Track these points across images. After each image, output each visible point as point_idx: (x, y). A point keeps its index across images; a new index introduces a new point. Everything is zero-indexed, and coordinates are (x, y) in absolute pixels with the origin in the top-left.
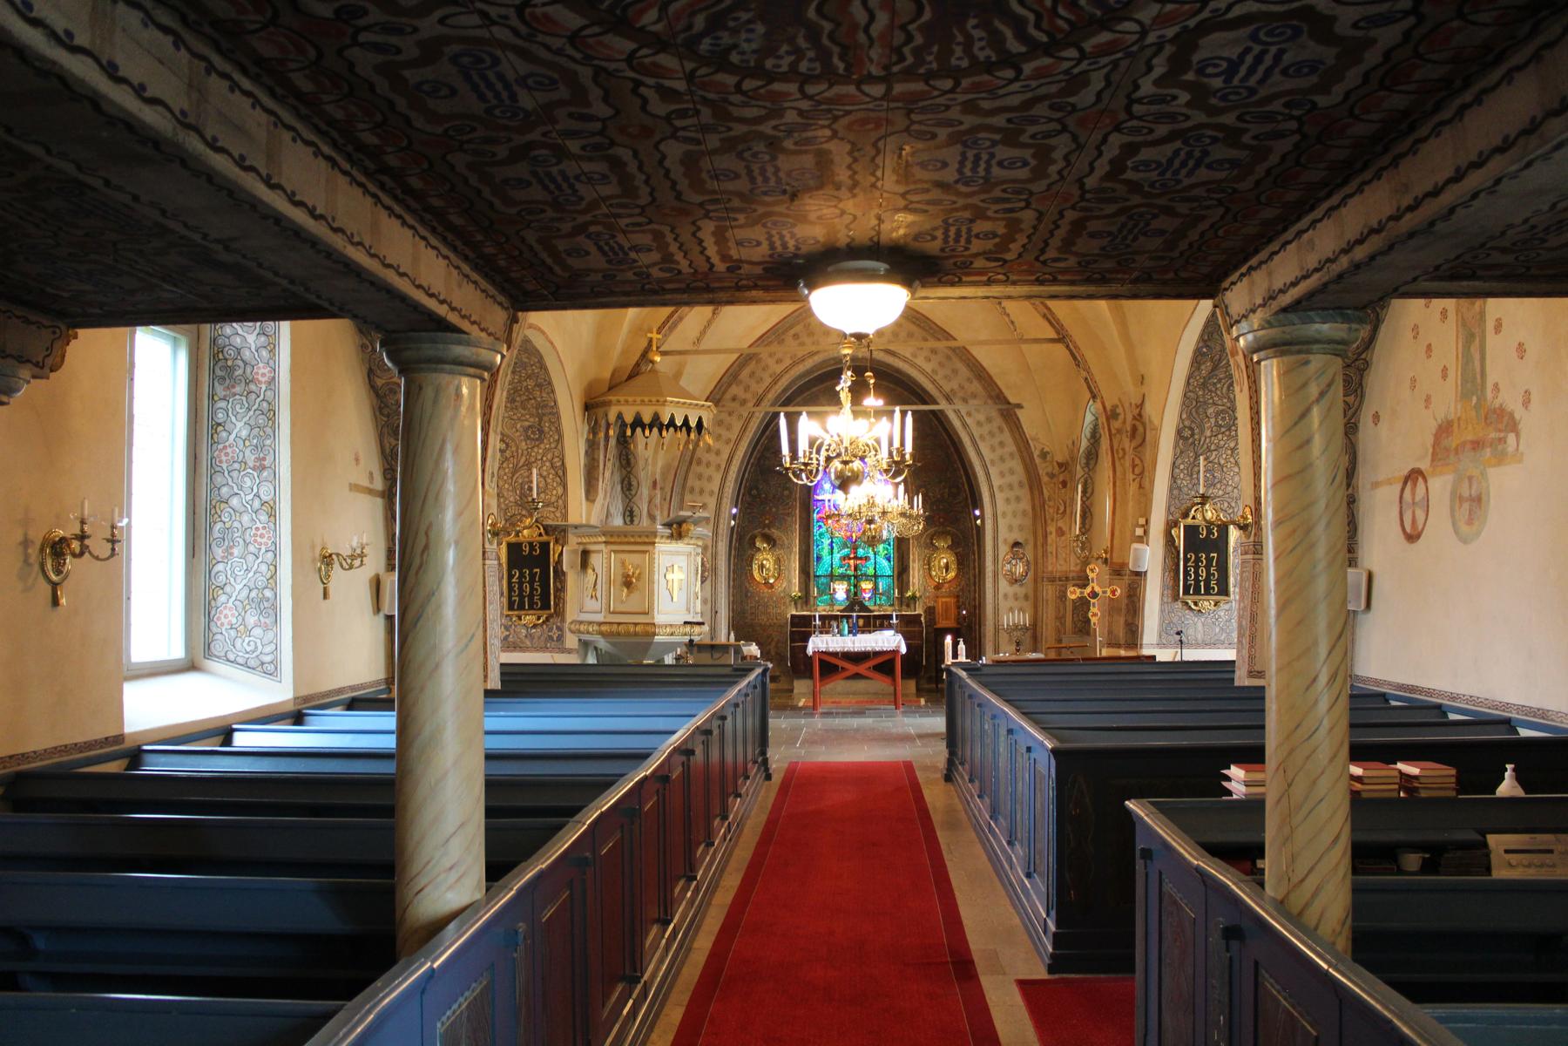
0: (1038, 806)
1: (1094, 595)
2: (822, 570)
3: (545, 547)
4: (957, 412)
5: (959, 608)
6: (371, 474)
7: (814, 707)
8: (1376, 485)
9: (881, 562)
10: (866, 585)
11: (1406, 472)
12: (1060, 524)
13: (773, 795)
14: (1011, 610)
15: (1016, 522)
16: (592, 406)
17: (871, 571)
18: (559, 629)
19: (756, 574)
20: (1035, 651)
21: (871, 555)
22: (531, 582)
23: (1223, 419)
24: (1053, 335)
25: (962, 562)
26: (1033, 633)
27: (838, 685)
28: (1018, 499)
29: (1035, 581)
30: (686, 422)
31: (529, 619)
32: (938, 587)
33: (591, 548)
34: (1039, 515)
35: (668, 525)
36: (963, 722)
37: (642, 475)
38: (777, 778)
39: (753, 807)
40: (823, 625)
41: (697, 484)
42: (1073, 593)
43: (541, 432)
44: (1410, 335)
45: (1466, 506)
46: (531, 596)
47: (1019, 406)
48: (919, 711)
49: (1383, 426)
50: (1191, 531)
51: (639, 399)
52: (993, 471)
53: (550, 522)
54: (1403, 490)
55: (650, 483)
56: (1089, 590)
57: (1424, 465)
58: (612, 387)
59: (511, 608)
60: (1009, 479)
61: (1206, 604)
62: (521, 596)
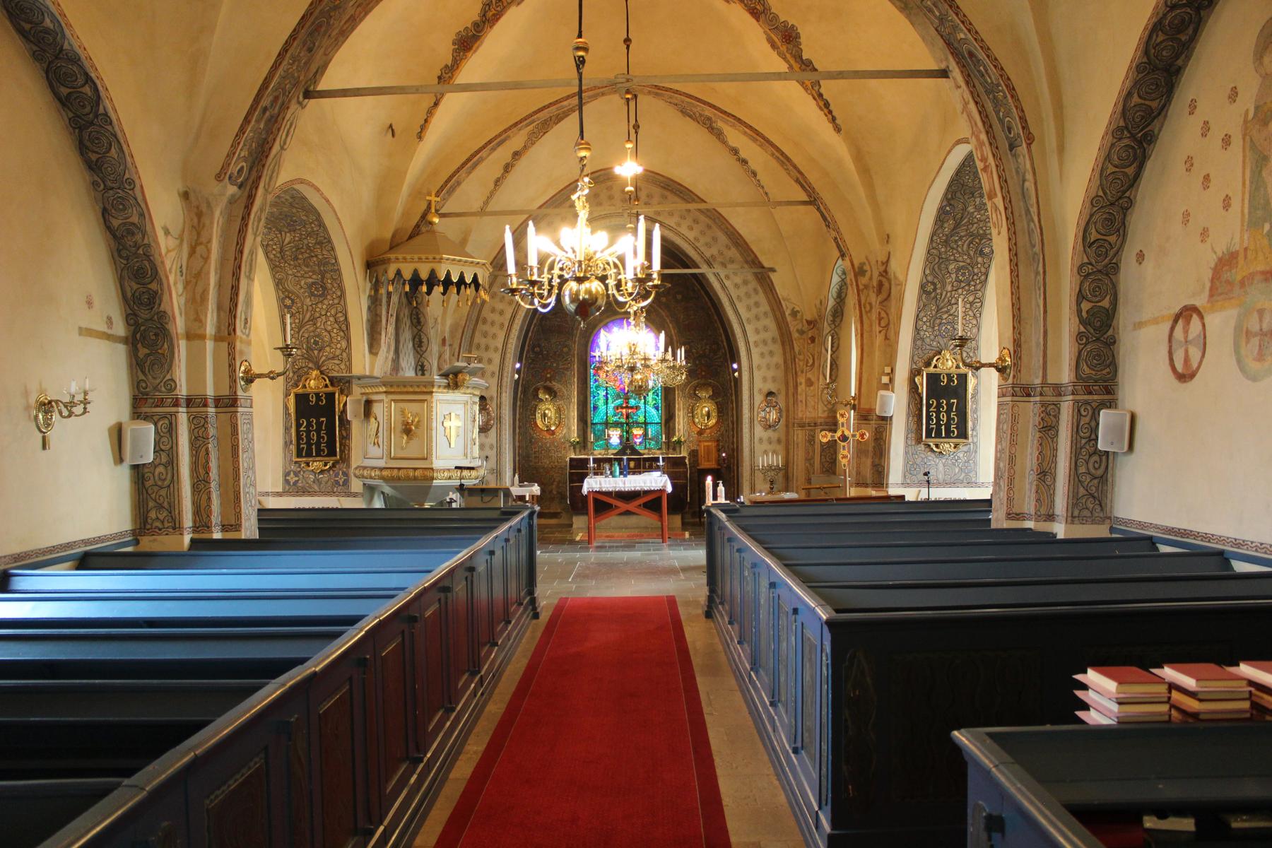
0: (807, 678)
1: (844, 438)
2: (598, 418)
3: (330, 397)
4: (717, 275)
5: (719, 451)
6: (109, 319)
7: (589, 542)
8: (1139, 325)
9: (651, 410)
10: (637, 432)
11: (1177, 309)
12: (809, 375)
13: (539, 634)
14: (766, 452)
15: (770, 374)
16: (373, 265)
17: (641, 419)
18: (345, 474)
19: (539, 422)
20: (787, 490)
21: (642, 404)
22: (318, 431)
23: (963, 274)
24: (803, 197)
25: (721, 410)
26: (784, 476)
27: (612, 520)
28: (771, 353)
29: (787, 426)
30: (462, 278)
31: (317, 465)
32: (701, 432)
33: (374, 397)
34: (790, 367)
35: (445, 375)
36: (723, 557)
37: (432, 333)
38: (545, 616)
39: (515, 653)
40: (599, 466)
41: (483, 341)
42: (825, 437)
43: (324, 288)
44: (1181, 167)
45: (1255, 341)
46: (318, 444)
47: (772, 270)
48: (682, 543)
49: (1149, 264)
50: (933, 379)
51: (416, 257)
52: (749, 328)
53: (335, 374)
54: (1172, 329)
55: (439, 340)
56: (839, 433)
57: (1200, 301)
58: (394, 246)
59: (299, 455)
60: (764, 335)
61: (947, 446)
62: (309, 444)
